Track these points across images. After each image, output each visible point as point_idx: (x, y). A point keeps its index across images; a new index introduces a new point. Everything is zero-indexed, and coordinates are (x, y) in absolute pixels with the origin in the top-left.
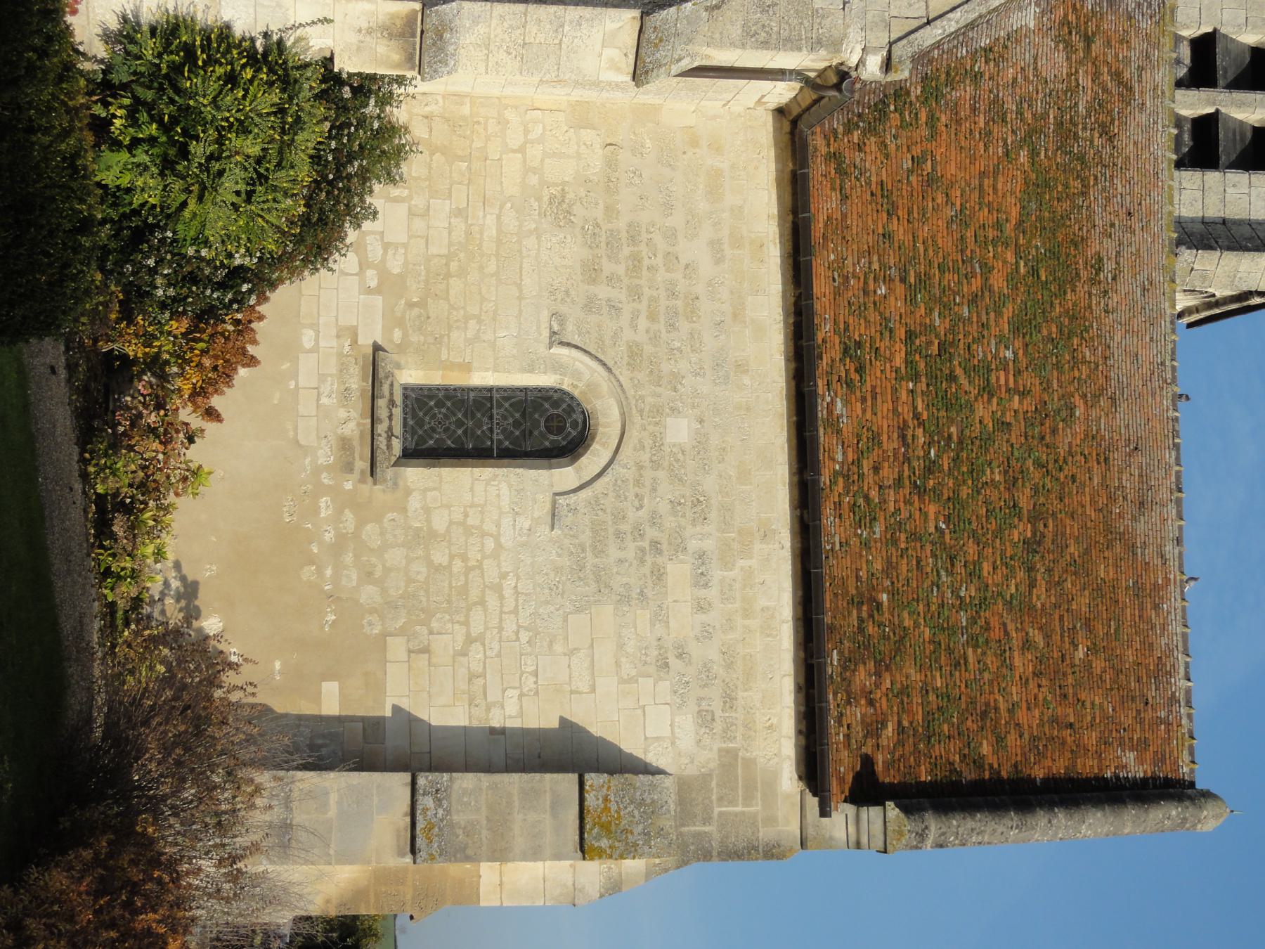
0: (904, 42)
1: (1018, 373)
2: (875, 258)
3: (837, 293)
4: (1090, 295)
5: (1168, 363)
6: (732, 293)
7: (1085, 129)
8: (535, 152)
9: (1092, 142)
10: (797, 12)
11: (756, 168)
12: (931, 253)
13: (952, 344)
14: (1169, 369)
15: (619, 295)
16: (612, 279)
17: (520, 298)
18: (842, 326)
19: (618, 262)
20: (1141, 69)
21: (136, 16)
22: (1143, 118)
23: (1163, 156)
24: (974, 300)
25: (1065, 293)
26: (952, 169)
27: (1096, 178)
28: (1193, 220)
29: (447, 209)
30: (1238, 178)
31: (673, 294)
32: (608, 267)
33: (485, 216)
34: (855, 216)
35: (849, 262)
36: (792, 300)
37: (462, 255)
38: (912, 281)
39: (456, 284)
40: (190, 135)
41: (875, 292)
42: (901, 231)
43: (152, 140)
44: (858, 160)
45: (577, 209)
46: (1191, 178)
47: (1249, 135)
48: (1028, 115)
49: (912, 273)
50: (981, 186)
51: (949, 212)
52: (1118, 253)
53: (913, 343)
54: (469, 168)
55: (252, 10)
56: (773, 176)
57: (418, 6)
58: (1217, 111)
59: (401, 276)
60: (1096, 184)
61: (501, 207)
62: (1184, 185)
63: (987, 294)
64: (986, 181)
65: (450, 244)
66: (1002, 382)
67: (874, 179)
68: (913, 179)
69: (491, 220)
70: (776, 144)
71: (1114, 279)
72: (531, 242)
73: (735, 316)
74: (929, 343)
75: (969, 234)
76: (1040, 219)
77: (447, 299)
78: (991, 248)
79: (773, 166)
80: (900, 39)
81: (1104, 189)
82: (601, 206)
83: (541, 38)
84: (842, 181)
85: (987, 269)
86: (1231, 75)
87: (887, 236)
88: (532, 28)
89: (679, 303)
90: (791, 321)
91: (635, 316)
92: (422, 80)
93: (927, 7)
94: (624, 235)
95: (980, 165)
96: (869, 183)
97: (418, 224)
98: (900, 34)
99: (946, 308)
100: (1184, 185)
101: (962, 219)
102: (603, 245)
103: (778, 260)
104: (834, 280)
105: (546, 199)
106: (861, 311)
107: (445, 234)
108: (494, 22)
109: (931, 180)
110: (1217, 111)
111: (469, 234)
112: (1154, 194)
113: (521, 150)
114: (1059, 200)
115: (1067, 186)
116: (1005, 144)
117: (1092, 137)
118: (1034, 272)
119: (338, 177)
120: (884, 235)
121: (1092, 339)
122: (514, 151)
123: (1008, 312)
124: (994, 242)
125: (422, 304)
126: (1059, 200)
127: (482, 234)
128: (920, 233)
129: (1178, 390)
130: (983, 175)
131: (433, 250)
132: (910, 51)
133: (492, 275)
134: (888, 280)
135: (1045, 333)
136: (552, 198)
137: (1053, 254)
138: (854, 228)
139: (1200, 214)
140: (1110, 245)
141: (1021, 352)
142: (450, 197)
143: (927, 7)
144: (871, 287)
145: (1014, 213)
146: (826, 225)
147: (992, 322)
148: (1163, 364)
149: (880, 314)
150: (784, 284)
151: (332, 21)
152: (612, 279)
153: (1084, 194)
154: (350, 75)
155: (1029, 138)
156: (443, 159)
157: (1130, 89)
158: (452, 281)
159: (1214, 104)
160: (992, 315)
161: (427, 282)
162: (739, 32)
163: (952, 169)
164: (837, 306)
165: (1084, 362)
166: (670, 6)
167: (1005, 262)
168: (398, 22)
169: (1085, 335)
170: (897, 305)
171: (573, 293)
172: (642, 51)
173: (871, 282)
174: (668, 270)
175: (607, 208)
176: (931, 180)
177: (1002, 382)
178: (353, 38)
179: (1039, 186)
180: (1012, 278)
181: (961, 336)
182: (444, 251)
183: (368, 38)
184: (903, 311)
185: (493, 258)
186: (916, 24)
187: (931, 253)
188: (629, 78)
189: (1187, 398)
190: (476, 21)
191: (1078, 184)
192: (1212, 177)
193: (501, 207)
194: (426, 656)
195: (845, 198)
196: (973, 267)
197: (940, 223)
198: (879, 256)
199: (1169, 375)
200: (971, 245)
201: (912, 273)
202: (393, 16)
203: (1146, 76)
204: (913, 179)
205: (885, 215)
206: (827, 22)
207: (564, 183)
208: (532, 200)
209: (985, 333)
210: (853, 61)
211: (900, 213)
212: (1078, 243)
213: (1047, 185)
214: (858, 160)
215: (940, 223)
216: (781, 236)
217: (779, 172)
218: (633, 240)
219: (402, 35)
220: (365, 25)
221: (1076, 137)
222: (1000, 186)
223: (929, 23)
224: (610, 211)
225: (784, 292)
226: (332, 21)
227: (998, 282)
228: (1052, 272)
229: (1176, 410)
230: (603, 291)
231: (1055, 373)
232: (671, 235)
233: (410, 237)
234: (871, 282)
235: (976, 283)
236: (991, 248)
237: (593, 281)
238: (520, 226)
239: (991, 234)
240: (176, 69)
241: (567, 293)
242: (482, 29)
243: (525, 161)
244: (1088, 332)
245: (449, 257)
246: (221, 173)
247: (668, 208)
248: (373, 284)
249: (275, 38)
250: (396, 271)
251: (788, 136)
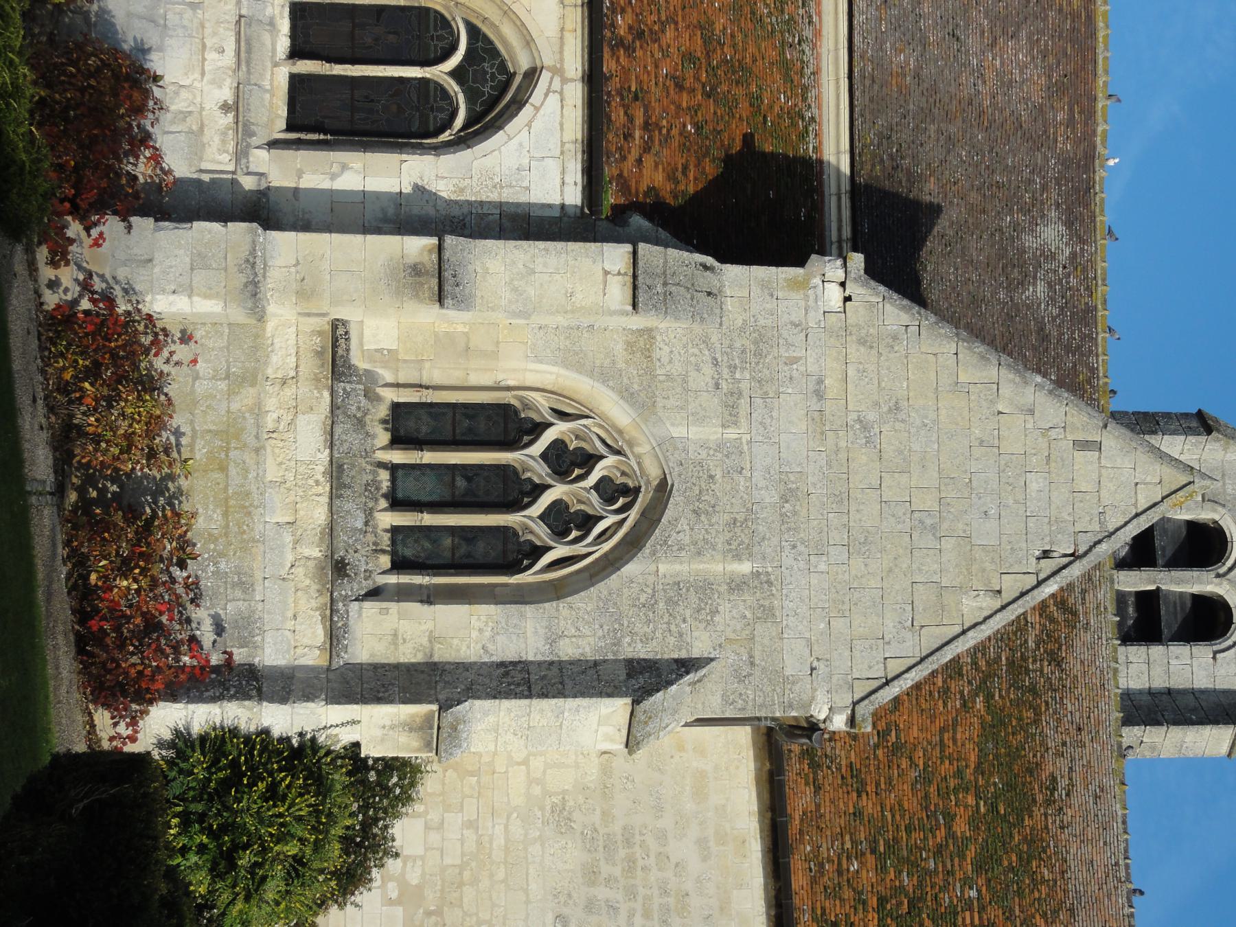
0: (866, 702)
1: (982, 909)
2: (847, 838)
3: (814, 881)
4: (1046, 815)
5: (1121, 862)
6: (718, 888)
7: (1035, 661)
8: (537, 764)
9: (1042, 671)
10: (770, 680)
11: (737, 768)
12: (898, 817)
13: (920, 899)
14: (1122, 868)
15: (616, 895)
16: (609, 881)
17: (528, 902)
18: (819, 912)
19: (614, 864)
20: (1084, 592)
21: (187, 729)
22: (1088, 637)
23: (1109, 667)
24: (939, 851)
25: (1023, 820)
26: (915, 732)
27: (1047, 703)
28: (1141, 692)
29: (460, 821)
30: (1180, 652)
31: (666, 892)
32: (606, 870)
33: (494, 826)
34: (828, 804)
35: (823, 849)
36: (773, 893)
37: (474, 864)
38: (882, 849)
39: (469, 893)
40: (237, 847)
41: (848, 870)
42: (870, 805)
43: (202, 849)
44: (829, 750)
45: (576, 815)
46: (1136, 653)
47: (1189, 604)
48: (982, 663)
49: (882, 842)
50: (942, 740)
51: (913, 774)
52: (1071, 768)
53: (884, 908)
54: (478, 782)
55: (288, 718)
56: (752, 775)
57: (435, 707)
58: (1158, 588)
59: (419, 887)
60: (1047, 709)
61: (508, 818)
62: (1131, 659)
63: (951, 841)
64: (946, 736)
65: (463, 854)
66: (968, 921)
67: (844, 763)
68: (880, 752)
69: (499, 830)
70: (754, 744)
71: (1068, 795)
72: (535, 849)
73: (722, 909)
74: (899, 904)
75: (932, 789)
76: (996, 756)
77: (461, 906)
78: (952, 797)
79: (752, 765)
80: (862, 699)
81: (1055, 712)
82: (598, 812)
83: (544, 722)
84: (815, 774)
85: (950, 817)
86: (1169, 552)
87: (858, 814)
88: (536, 716)
89: (671, 900)
90: (773, 913)
91: (631, 915)
92: (439, 762)
93: (885, 668)
94: (619, 838)
95: (939, 723)
96: (839, 769)
97: (434, 837)
98: (862, 695)
99: (914, 865)
100: (1131, 659)
101: (926, 778)
102: (601, 848)
103: (760, 855)
104: (811, 870)
105: (548, 808)
106: (833, 893)
107: (458, 845)
108: (502, 714)
109: (896, 749)
110: (1158, 588)
111: (479, 843)
112: (1102, 705)
113: (525, 762)
114: (1013, 734)
115: (1020, 719)
116: (962, 693)
117: (1042, 666)
118: (993, 808)
119: (364, 838)
120: (854, 814)
121: (1050, 858)
122: (519, 764)
123: (970, 854)
124: (956, 790)
125: (438, 912)
126: (1013, 734)
127: (491, 843)
128: (888, 802)
129: (1132, 887)
130: (943, 730)
131: (448, 861)
132: (872, 709)
133: (502, 881)
134: (860, 856)
135: (1006, 863)
136: (554, 806)
137: (1010, 787)
138: (827, 816)
139: (1147, 686)
140: (1063, 764)
141: (984, 889)
142: (462, 810)
143: (885, 668)
144: (845, 866)
145: (973, 758)
146: (802, 820)
147: (957, 868)
148: (1117, 864)
149: (854, 890)
150: (765, 877)
151: (359, 722)
152: (609, 881)
153: (1037, 721)
154: (376, 760)
155: (984, 688)
156: (455, 775)
157: (1075, 614)
158: (464, 889)
159: (1155, 582)
160: (956, 860)
161: (442, 891)
162: (719, 701)
163: (915, 732)
164: (814, 893)
165: (1043, 881)
166: (658, 691)
167: (966, 807)
168: (418, 720)
169: (1043, 855)
170: (869, 876)
171: (575, 895)
172: (633, 730)
173: (844, 861)
174: (659, 870)
175: (603, 813)
176: (896, 749)
177: (968, 921)
178: (379, 733)
179: (995, 726)
180: (974, 822)
181: (928, 889)
182: (459, 862)
183: (391, 732)
184: (874, 880)
185: (502, 866)
186: (876, 684)
187: (898, 817)
188: (622, 746)
189: (1142, 893)
190: (486, 714)
191: (1031, 714)
192: (1157, 650)
193: (508, 818)
194: (400, 495)
195: (818, 789)
196: (937, 820)
197: (905, 787)
198: (851, 835)
199: (1123, 874)
200: (934, 798)
201: (882, 842)
202: (412, 716)
203: (1089, 597)
204: (880, 752)
205: (855, 795)
206: (797, 688)
207: (564, 792)
208: (536, 809)
209: (951, 880)
210: (822, 717)
211: (869, 789)
212: (1033, 769)
213: (1002, 723)
214: (829, 750)
215: (905, 787)
216: (761, 831)
217: (758, 771)
218: (628, 842)
219: (421, 728)
220: (388, 723)
221: (1027, 671)
222: (959, 736)
223: (887, 683)
224: (606, 815)
225: (766, 885)
226: (359, 722)
227: (961, 827)
228: (1009, 804)
229: (1131, 906)
230: (602, 893)
231: (1017, 899)
232: (662, 837)
233: (426, 850)
234: (844, 861)
235: (941, 834)
236: (952, 797)
237: (592, 883)
238: (526, 835)
239: (952, 783)
240: (225, 784)
241: (569, 896)
242: (491, 719)
243: (528, 773)
244: (1045, 852)
245: (461, 868)
246: (264, 879)
247: (659, 810)
248: (394, 895)
249: (309, 736)
250: (414, 882)
251: (765, 738)
